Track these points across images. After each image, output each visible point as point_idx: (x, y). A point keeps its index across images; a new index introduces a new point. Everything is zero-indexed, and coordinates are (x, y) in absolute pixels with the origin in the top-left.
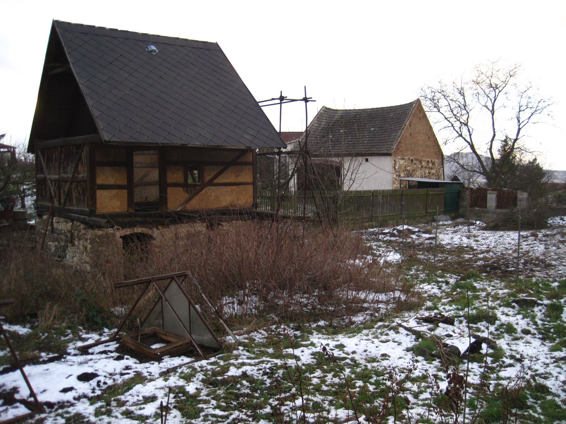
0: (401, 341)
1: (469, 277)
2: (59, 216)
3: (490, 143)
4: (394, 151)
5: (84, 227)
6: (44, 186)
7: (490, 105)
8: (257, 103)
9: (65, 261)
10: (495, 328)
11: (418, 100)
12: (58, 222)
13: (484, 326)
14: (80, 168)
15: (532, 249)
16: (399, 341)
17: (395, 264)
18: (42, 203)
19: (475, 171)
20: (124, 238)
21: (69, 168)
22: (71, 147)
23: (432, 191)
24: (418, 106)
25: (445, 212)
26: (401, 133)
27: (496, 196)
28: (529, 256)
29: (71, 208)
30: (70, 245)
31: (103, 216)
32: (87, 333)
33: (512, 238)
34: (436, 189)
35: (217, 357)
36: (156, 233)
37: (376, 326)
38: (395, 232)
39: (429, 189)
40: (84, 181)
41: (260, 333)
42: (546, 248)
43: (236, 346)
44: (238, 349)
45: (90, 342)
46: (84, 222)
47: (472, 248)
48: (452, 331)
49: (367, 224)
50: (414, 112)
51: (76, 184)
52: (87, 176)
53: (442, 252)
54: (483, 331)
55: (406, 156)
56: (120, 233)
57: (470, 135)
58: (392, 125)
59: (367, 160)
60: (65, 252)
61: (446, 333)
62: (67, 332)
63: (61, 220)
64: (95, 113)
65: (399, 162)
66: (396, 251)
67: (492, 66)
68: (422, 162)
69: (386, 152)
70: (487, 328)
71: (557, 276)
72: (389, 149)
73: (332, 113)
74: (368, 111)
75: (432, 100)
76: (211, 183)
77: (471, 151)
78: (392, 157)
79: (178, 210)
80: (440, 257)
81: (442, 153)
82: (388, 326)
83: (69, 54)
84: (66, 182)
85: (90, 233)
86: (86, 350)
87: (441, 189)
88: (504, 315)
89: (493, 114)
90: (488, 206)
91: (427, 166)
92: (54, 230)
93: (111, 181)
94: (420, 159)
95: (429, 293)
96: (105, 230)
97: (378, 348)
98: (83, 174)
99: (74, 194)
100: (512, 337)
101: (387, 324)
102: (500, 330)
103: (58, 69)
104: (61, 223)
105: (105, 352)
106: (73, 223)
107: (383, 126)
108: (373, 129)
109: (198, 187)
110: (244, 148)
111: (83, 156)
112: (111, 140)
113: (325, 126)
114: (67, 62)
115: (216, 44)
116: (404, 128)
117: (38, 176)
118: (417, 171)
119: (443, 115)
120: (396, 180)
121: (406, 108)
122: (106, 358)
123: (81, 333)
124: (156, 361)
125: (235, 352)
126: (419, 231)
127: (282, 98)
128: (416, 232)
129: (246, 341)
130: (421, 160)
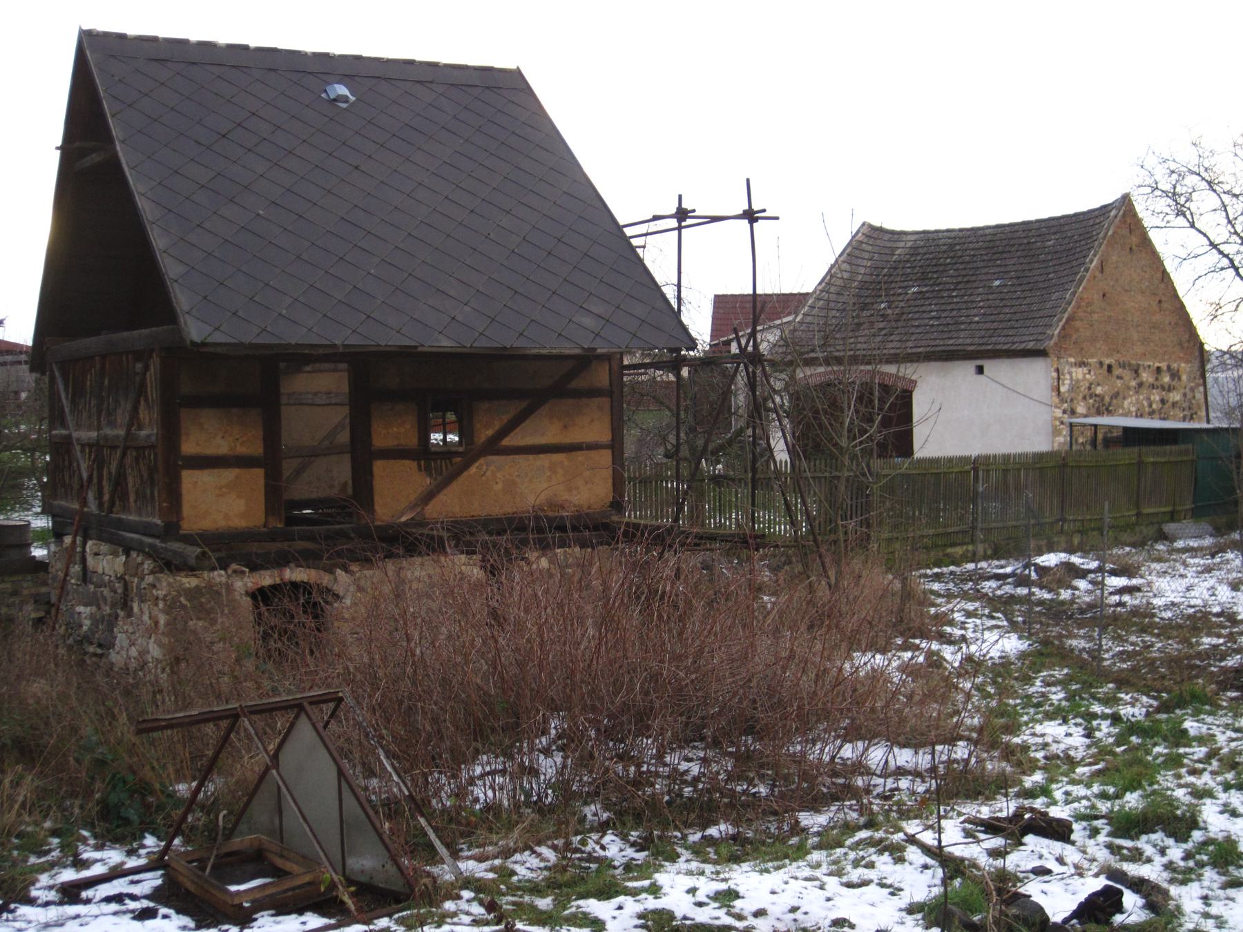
0: (902, 885)
1: (1181, 703)
2: (100, 539)
4: (1056, 344)
5: (152, 566)
6: (66, 458)
8: (620, 228)
9: (115, 657)
10: (1185, 850)
11: (1126, 200)
12: (97, 554)
13: (1155, 846)
14: (143, 414)
16: (896, 885)
17: (994, 664)
18: (63, 503)
20: (261, 596)
21: (119, 411)
22: (124, 358)
23: (1152, 455)
24: (1124, 216)
25: (1197, 514)
26: (1074, 293)
29: (124, 517)
30: (121, 614)
31: (189, 539)
32: (99, 848)
34: (1168, 448)
35: (396, 916)
36: (342, 581)
37: (848, 842)
39: (1144, 449)
40: (152, 447)
41: (539, 855)
43: (455, 888)
44: (459, 897)
45: (97, 870)
46: (153, 554)
48: (1057, 859)
49: (959, 550)
50: (1114, 233)
51: (134, 454)
52: (157, 433)
53: (1143, 630)
54: (1149, 860)
55: (1092, 357)
56: (245, 583)
58: (1051, 270)
59: (980, 370)
60: (112, 631)
61: (1037, 863)
62: (49, 844)
63: (104, 548)
64: (171, 268)
65: (1070, 373)
66: (1014, 627)
68: (1141, 371)
69: (1031, 345)
70: (1163, 852)
73: (889, 241)
74: (987, 232)
75: (1174, 195)
76: (493, 447)
78: (1049, 360)
79: (404, 519)
80: (1132, 644)
81: (1202, 344)
82: (881, 840)
83: (113, 116)
84: (114, 448)
85: (166, 584)
86: (75, 890)
87: (1183, 447)
88: (1226, 815)
91: (1156, 383)
92: (89, 574)
93: (221, 446)
94: (1134, 362)
95: (1054, 748)
96: (206, 574)
97: (831, 903)
98: (149, 432)
99: (130, 480)
100: (1224, 878)
101: (879, 834)
102: (1198, 857)
103: (94, 155)
104: (101, 557)
105: (118, 898)
106: (128, 555)
107: (1027, 273)
108: (997, 283)
109: (458, 460)
110: (577, 351)
111: (148, 381)
112: (209, 340)
113: (867, 278)
114: (110, 140)
115: (518, 74)
116: (1083, 277)
117: (54, 432)
118: (1124, 398)
119: (1205, 235)
120: (1062, 423)
121: (1091, 222)
122: (115, 913)
123: (81, 848)
124: (235, 925)
125: (449, 905)
126: (1100, 569)
127: (682, 214)
128: (1090, 571)
129: (491, 875)
130: (1138, 365)
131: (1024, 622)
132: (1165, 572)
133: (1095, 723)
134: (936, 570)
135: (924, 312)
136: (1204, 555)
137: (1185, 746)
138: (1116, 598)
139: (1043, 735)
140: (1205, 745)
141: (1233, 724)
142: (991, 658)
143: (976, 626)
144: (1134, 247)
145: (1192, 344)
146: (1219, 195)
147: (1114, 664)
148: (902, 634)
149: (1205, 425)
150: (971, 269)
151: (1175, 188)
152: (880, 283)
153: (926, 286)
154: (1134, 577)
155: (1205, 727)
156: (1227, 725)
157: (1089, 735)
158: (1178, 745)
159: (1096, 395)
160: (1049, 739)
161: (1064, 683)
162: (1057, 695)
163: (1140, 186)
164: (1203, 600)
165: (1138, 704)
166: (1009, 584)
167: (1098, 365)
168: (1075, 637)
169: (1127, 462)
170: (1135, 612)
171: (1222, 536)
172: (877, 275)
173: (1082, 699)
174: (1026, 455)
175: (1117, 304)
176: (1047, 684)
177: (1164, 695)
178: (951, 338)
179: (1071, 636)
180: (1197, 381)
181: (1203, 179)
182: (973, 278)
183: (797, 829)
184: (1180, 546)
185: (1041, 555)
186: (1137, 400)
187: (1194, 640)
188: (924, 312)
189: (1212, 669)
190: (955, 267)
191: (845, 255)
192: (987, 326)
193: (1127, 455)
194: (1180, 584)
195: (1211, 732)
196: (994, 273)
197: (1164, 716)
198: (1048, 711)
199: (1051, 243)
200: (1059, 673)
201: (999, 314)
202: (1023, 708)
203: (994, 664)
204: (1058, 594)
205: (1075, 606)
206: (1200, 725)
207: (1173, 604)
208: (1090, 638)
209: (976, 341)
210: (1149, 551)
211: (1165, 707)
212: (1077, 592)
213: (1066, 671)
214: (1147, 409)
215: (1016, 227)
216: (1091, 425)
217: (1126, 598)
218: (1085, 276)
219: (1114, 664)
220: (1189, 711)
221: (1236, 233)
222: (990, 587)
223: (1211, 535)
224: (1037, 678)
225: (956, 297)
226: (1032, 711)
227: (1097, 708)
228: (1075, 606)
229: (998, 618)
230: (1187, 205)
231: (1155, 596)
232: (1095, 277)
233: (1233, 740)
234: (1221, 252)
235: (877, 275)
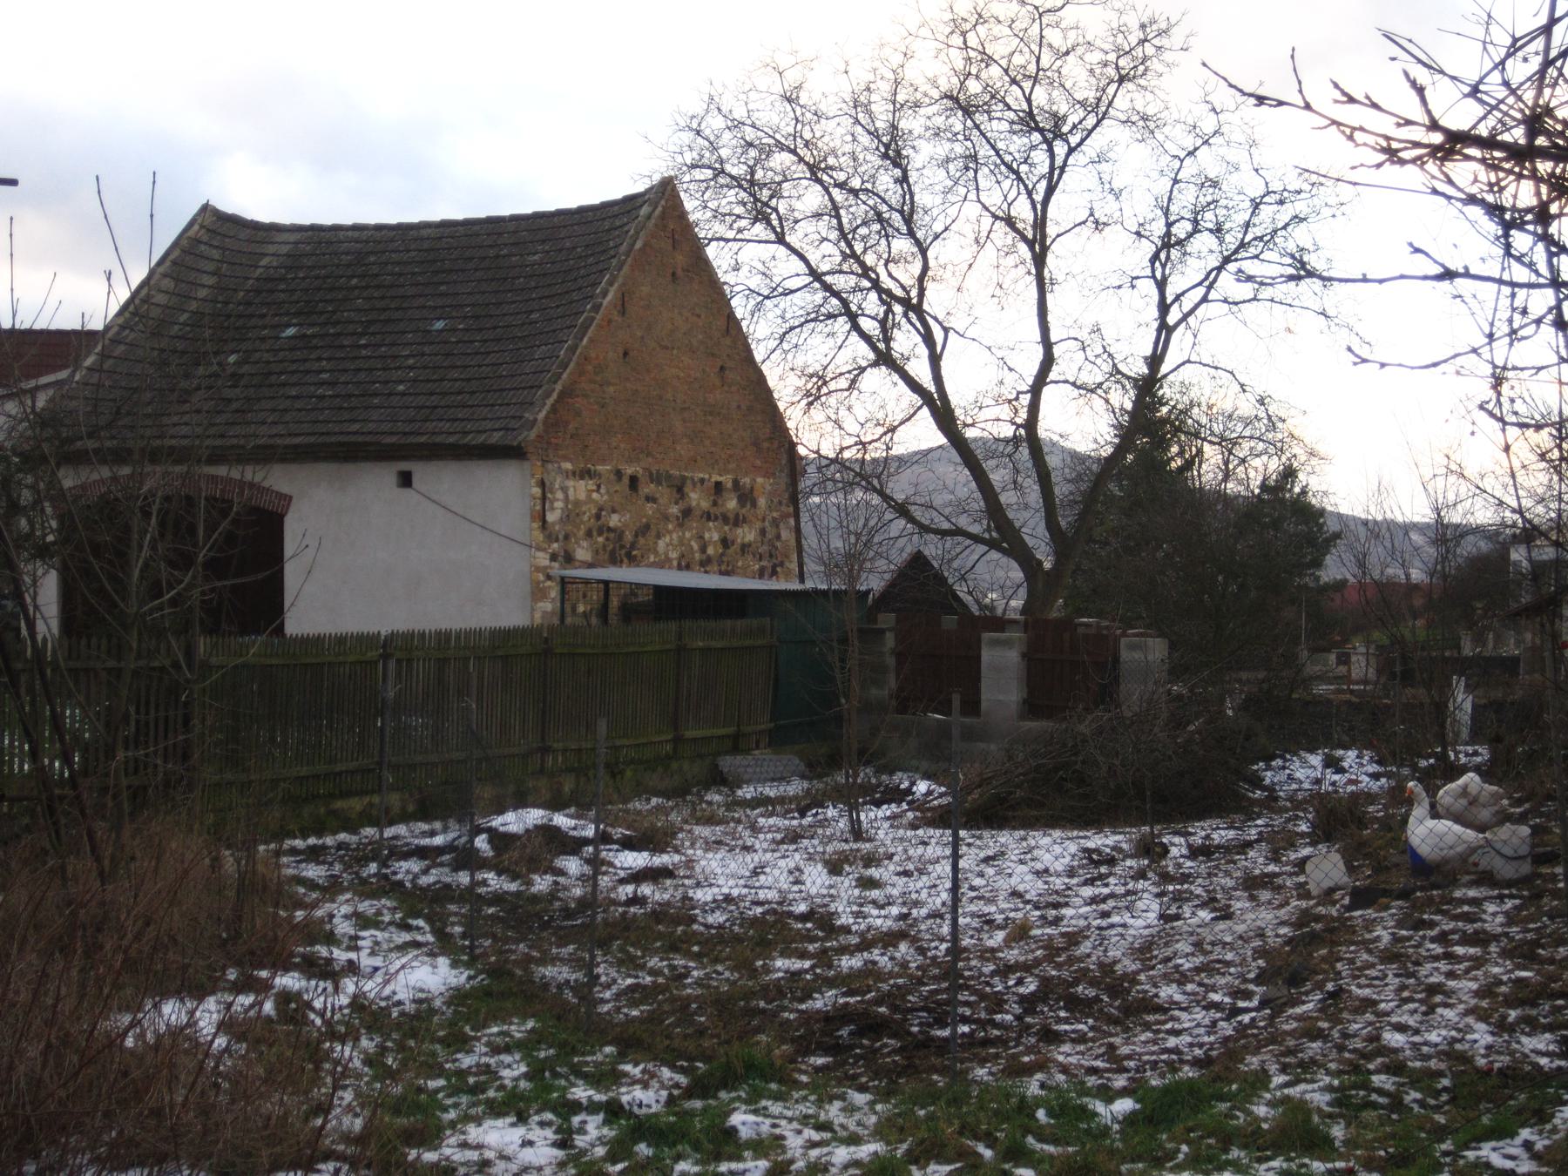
1: (728, 1079)
3: (1026, 399)
7: (1023, 211)
11: (666, 190)
15: (1104, 923)
17: (402, 1014)
19: (958, 532)
23: (701, 635)
24: (663, 216)
25: (778, 739)
26: (573, 349)
27: (1024, 655)
28: (1071, 961)
33: (1039, 866)
38: (481, 842)
42: (1163, 917)
47: (822, 919)
49: (356, 804)
50: (645, 245)
53: (674, 946)
55: (604, 461)
57: (935, 360)
59: (406, 480)
65: (564, 490)
66: (444, 945)
67: (1036, 26)
69: (495, 438)
71: (1154, 1065)
72: (514, 424)
74: (424, 233)
75: (750, 184)
77: (941, 439)
78: (526, 465)
89: (1040, 260)
90: (984, 705)
108: (440, 325)
118: (658, 537)
120: (549, 577)
121: (607, 224)
126: (603, 838)
130: (684, 479)
131: (464, 936)
132: (719, 843)
133: (576, 1120)
134: (312, 841)
135: (307, 372)
136: (790, 811)
137: (731, 1158)
138: (630, 889)
139: (479, 1147)
140: (766, 1156)
141: (816, 1117)
142: (399, 1003)
143: (377, 943)
144: (679, 272)
145: (776, 445)
146: (826, 189)
147: (618, 1010)
148: (238, 964)
149: (795, 586)
150: (393, 298)
151: (752, 174)
152: (229, 316)
153: (312, 325)
154: (663, 851)
155: (768, 1121)
156: (806, 1117)
157: (563, 1143)
158: (718, 1157)
159: (610, 529)
160: (489, 1155)
161: (525, 1047)
162: (513, 1070)
163: (694, 166)
164: (780, 891)
165: (655, 1083)
166: (442, 865)
167: (612, 477)
168: (554, 960)
169: (657, 648)
170: (660, 914)
171: (820, 777)
172: (226, 303)
173: (556, 1075)
174: (479, 633)
175: (648, 371)
176: (496, 1050)
177: (700, 1065)
178: (354, 421)
179: (547, 960)
180: (784, 508)
181: (801, 160)
182: (398, 315)
183: (595, 1067)
184: (748, 796)
185: (501, 812)
186: (681, 539)
187: (760, 963)
188: (307, 372)
189: (786, 1015)
190: (365, 294)
191: (168, 263)
192: (421, 400)
193: (656, 636)
194: (740, 864)
195: (777, 1131)
196: (435, 308)
197: (698, 1104)
198: (494, 1099)
199: (536, 257)
200: (519, 1029)
201: (442, 380)
202: (449, 1096)
203: (402, 1014)
204: (530, 883)
205: (557, 904)
206: (760, 1119)
207: (728, 899)
208: (575, 962)
209: (400, 427)
210: (693, 803)
211: (699, 1088)
212: (561, 880)
213: (530, 1024)
214: (697, 556)
215: (476, 228)
216: (599, 581)
217: (646, 889)
218: (593, 319)
219: (618, 1010)
220: (743, 1095)
221: (854, 255)
222: (408, 872)
223: (803, 777)
224: (478, 1039)
225: (365, 346)
226: (464, 1099)
227: (581, 1093)
228: (557, 904)
229: (418, 928)
230: (773, 203)
231: (698, 885)
232: (610, 321)
233: (813, 1145)
234: (827, 287)
235: (226, 303)
